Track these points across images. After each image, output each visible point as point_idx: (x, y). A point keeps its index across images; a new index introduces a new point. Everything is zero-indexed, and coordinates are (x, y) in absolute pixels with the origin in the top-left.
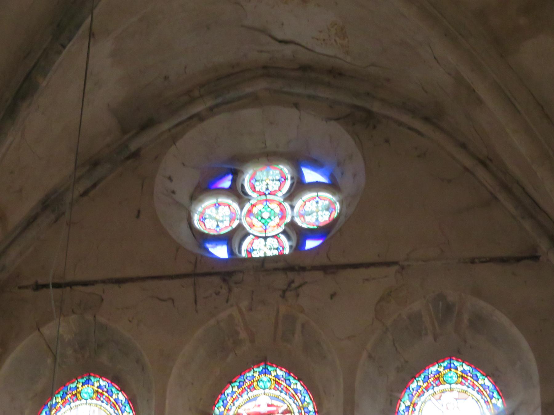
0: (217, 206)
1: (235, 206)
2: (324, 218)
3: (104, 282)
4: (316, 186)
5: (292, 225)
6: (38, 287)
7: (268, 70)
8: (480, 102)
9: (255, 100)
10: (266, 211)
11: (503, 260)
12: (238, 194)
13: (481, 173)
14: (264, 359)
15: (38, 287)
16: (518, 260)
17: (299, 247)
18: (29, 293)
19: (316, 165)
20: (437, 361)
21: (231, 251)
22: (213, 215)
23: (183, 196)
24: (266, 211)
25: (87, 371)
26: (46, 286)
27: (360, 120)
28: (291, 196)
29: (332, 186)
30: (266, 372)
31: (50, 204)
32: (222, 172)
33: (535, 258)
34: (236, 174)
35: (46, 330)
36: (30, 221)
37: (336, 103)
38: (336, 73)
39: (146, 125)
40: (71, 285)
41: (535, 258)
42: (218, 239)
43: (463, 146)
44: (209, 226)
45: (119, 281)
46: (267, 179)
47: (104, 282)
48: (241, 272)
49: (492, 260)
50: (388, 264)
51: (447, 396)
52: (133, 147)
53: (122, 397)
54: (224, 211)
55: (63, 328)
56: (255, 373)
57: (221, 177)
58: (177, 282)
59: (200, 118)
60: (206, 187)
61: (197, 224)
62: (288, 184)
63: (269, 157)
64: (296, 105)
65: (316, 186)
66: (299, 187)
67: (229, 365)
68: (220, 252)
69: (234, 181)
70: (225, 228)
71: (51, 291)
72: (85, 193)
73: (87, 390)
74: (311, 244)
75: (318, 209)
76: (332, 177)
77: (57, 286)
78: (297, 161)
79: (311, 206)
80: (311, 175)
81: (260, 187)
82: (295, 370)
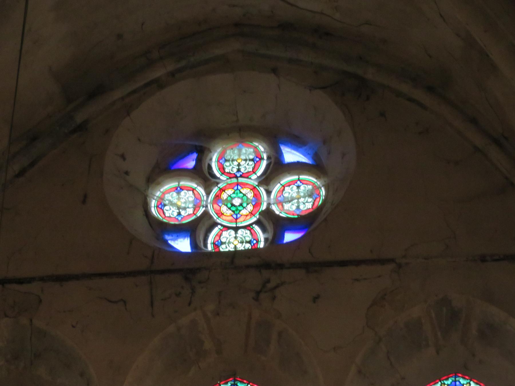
0: (179, 190)
1: (201, 190)
2: (307, 205)
3: (42, 279)
5: (268, 213)
12: (205, 177)
17: (275, 240)
19: (297, 143)
21: (194, 244)
22: (175, 200)
27: (351, 90)
29: (316, 168)
32: (184, 152)
34: (202, 152)
38: (322, 33)
39: (96, 92)
42: (179, 230)
43: (474, 121)
44: (170, 213)
45: (61, 279)
46: (239, 158)
47: (42, 279)
48: (206, 265)
54: (187, 196)
59: (159, 84)
60: (165, 168)
61: (154, 211)
63: (242, 132)
64: (274, 71)
65: (297, 167)
66: (277, 169)
68: (183, 245)
69: (199, 161)
70: (188, 214)
72: (21, 173)
74: (289, 237)
75: (298, 196)
76: (316, 157)
78: (275, 138)
79: (290, 192)
80: (291, 155)
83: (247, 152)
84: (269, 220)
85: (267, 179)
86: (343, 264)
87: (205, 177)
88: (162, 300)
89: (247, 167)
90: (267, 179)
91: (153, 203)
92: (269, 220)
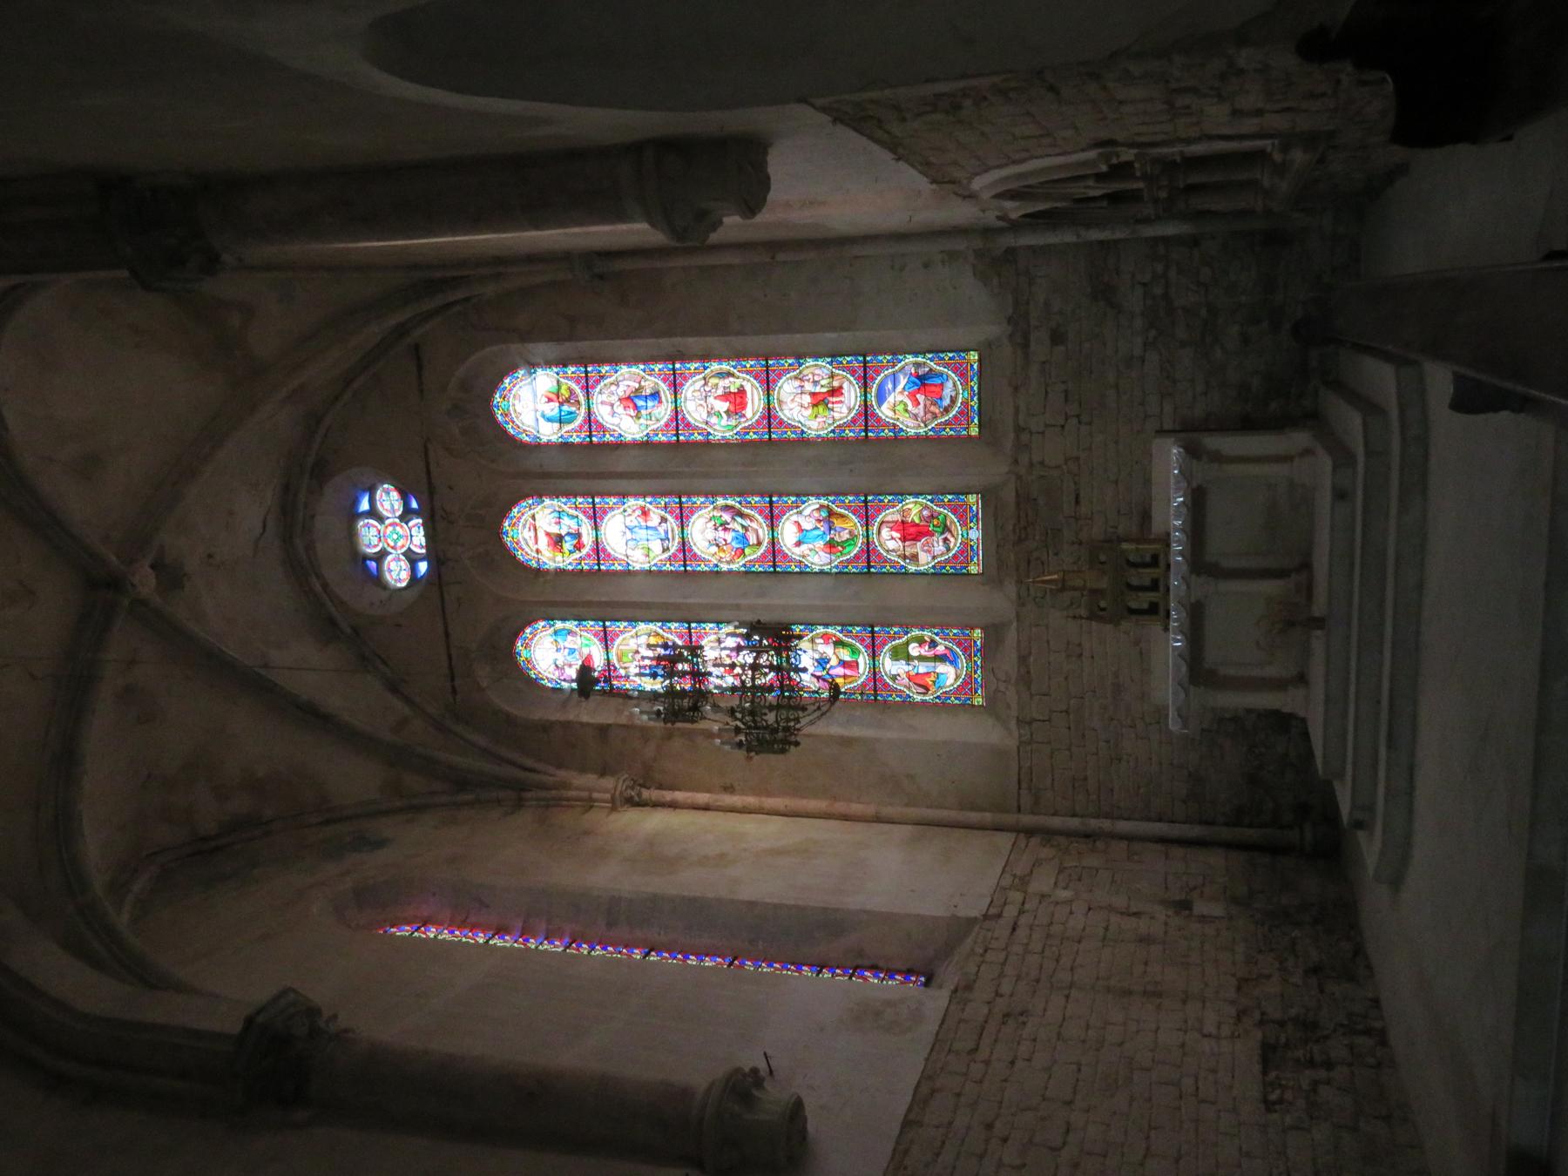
0: (390, 571)
1: (389, 558)
2: (395, 495)
3: (448, 647)
4: (372, 502)
5: (401, 518)
6: (454, 691)
7: (287, 539)
8: (907, 805)
9: (310, 547)
10: (392, 536)
11: (420, 368)
12: (382, 555)
13: (355, 385)
14: (497, 534)
15: (454, 691)
16: (419, 359)
17: (416, 513)
18: (458, 697)
19: (356, 502)
20: (493, 415)
21: (422, 560)
22: (397, 573)
23: (384, 595)
24: (392, 536)
25: (511, 655)
26: (454, 688)
27: (321, 472)
28: (381, 519)
29: (372, 491)
30: (506, 533)
31: (394, 688)
32: (365, 569)
33: (417, 347)
34: (366, 558)
35: (484, 684)
36: (408, 700)
37: (311, 486)
38: (286, 488)
39: (332, 622)
40: (451, 667)
41: (417, 347)
42: (414, 569)
43: (337, 398)
44: (405, 576)
45: (447, 635)
46: (369, 536)
47: (448, 647)
48: (436, 550)
49: (420, 376)
50: (426, 448)
51: (518, 408)
52: (349, 630)
53: (528, 631)
54: (393, 566)
55: (483, 673)
56: (508, 540)
57: (366, 569)
58: (446, 597)
59: (325, 586)
60: (378, 581)
61: (404, 584)
62: (372, 521)
63: (352, 535)
64: (313, 517)
65: (372, 502)
66: (373, 513)
67: (502, 558)
68: (423, 567)
69: (371, 559)
70: (404, 564)
71: (457, 682)
72: (385, 663)
73: (524, 653)
74: (414, 505)
75: (389, 500)
76: (364, 491)
77: (453, 680)
78: (355, 516)
79: (387, 505)
80: (364, 505)
81: (375, 541)
82: (504, 512)
83: (364, 531)
84: (406, 515)
85: (381, 519)
86: (428, 472)
87: (382, 555)
88: (1066, 400)
89: (373, 531)
90: (381, 519)
91: (725, 367)
92: (406, 515)
